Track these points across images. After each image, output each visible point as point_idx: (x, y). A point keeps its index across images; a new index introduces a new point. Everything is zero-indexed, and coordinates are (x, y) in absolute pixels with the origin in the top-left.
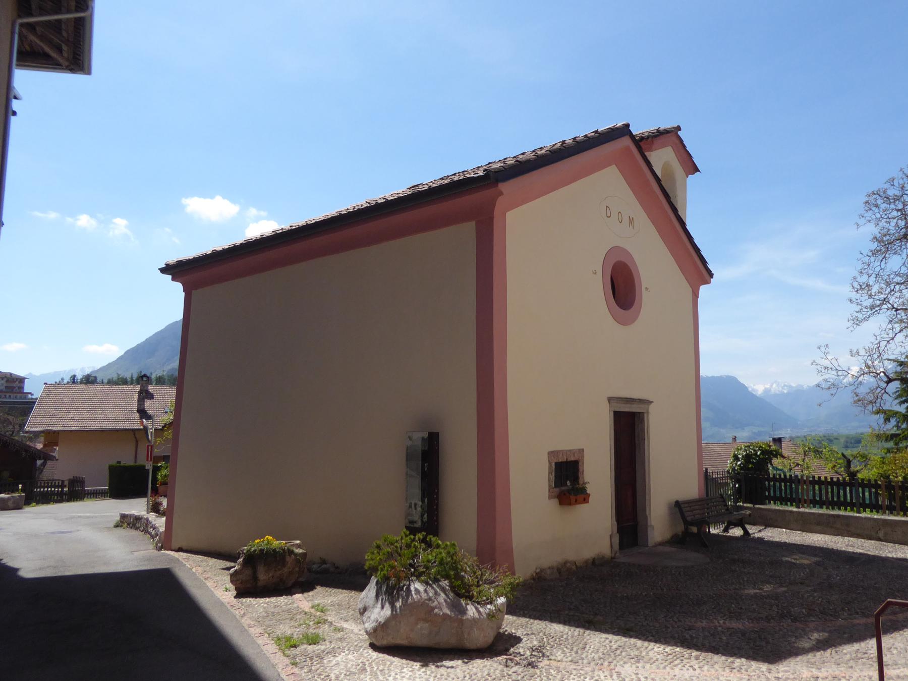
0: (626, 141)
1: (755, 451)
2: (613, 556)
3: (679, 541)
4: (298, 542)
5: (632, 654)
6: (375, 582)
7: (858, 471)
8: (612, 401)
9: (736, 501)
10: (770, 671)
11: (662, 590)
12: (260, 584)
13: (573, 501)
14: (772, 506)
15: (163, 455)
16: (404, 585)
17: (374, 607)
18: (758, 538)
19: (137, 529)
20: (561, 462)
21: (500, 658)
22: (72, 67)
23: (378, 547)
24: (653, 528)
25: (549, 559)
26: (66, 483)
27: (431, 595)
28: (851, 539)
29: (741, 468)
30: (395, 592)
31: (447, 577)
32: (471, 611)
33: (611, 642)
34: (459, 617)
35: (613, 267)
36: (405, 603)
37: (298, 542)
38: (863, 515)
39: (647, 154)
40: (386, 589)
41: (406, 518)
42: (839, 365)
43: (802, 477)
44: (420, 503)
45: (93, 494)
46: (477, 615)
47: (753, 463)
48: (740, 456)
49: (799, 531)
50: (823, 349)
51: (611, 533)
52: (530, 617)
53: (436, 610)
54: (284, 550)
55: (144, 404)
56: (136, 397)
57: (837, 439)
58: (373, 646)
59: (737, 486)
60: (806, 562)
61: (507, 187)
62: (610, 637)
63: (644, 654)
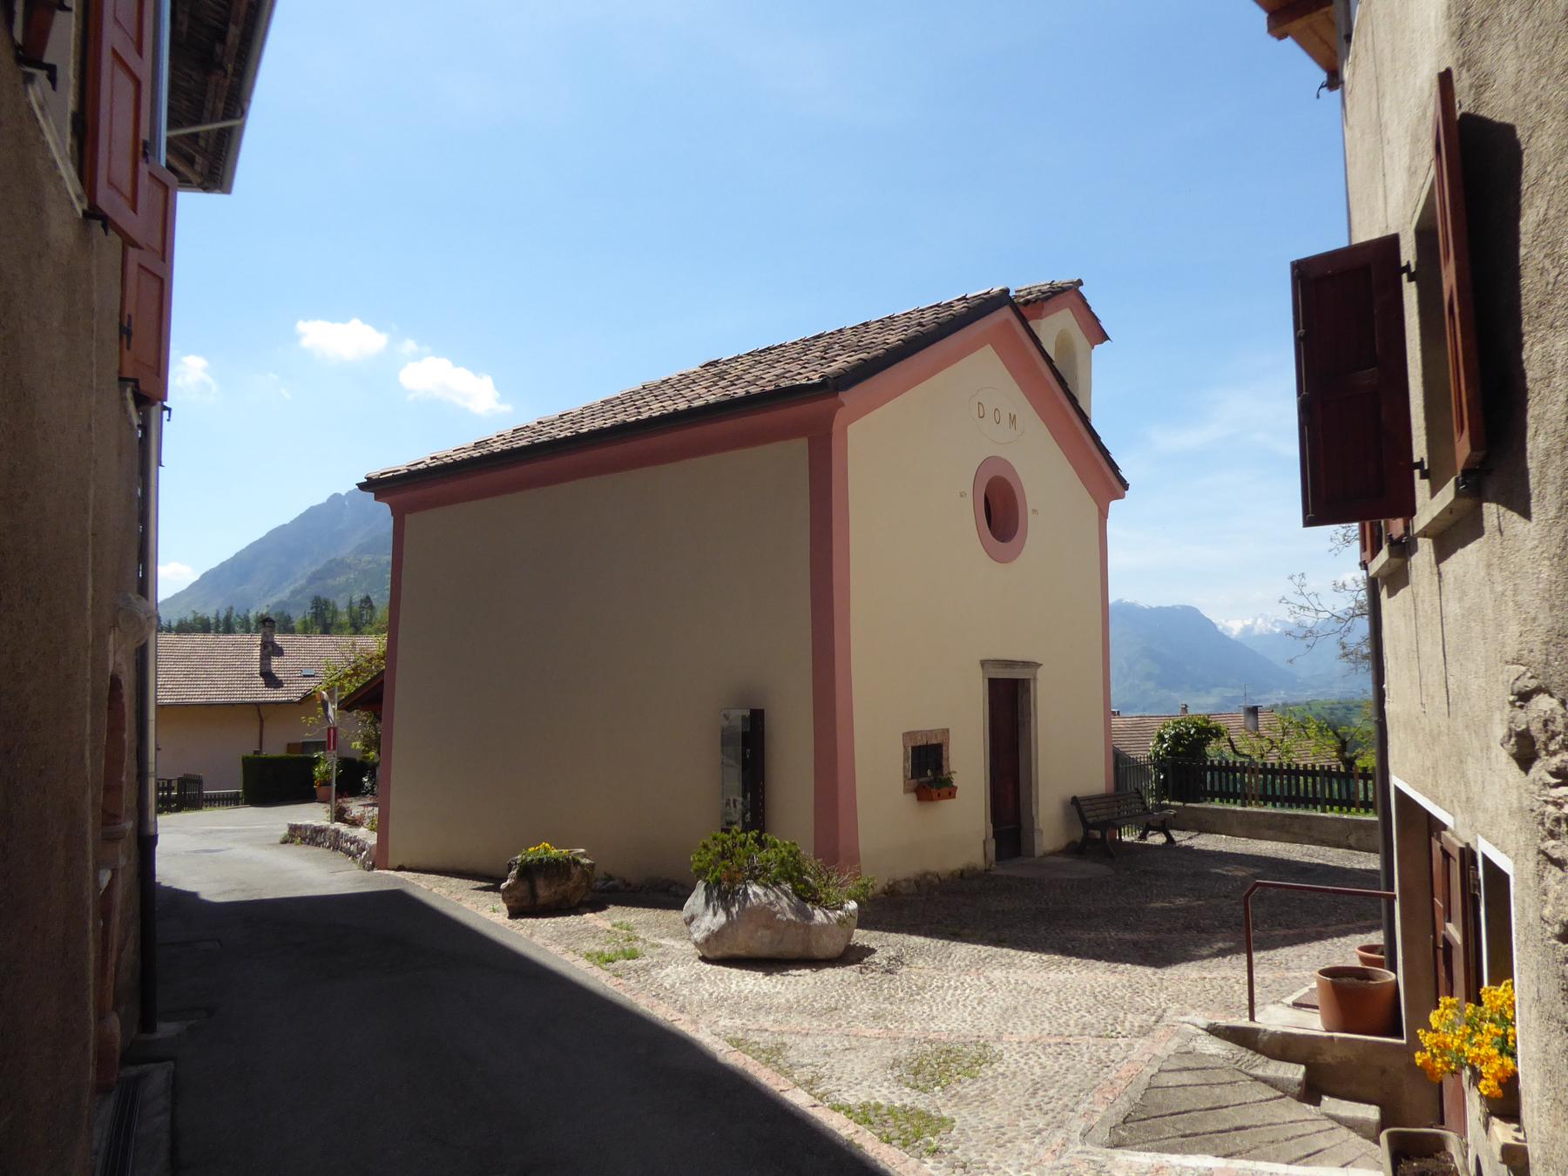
0: (1006, 313)
1: (1187, 728)
2: (987, 868)
3: (1075, 850)
4: (582, 850)
5: (1003, 962)
6: (703, 888)
7: (1356, 757)
8: (986, 665)
9: (1160, 798)
10: (1155, 974)
11: (1047, 904)
12: (540, 901)
13: (935, 795)
14: (1217, 805)
15: (301, 741)
16: (740, 889)
17: (703, 915)
18: (1186, 846)
19: (318, 845)
20: (920, 746)
21: (854, 967)
22: (206, 184)
23: (705, 846)
24: (1042, 833)
25: (906, 868)
26: (174, 784)
27: (772, 898)
28: (1313, 847)
29: (1168, 753)
30: (729, 896)
31: (790, 879)
32: (819, 916)
33: (980, 952)
34: (806, 922)
35: (988, 484)
36: (742, 908)
37: (582, 850)
38: (1329, 815)
39: (1032, 323)
40: (718, 894)
41: (722, 819)
42: (1319, 604)
43: (1281, 765)
44: (740, 799)
45: (231, 799)
46: (825, 921)
47: (1183, 746)
48: (1166, 736)
49: (1243, 837)
50: (1297, 580)
51: (983, 838)
52: (884, 930)
53: (779, 915)
54: (568, 859)
55: (270, 664)
56: (257, 652)
57: (1359, 707)
58: (704, 959)
59: (1162, 777)
60: (1241, 874)
61: (848, 397)
62: (980, 947)
63: (1017, 961)
